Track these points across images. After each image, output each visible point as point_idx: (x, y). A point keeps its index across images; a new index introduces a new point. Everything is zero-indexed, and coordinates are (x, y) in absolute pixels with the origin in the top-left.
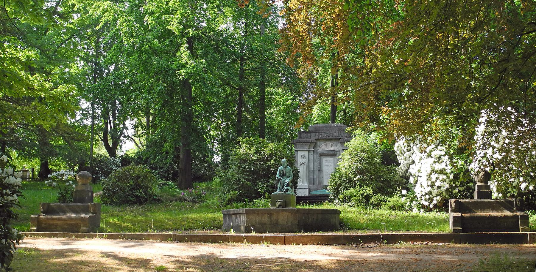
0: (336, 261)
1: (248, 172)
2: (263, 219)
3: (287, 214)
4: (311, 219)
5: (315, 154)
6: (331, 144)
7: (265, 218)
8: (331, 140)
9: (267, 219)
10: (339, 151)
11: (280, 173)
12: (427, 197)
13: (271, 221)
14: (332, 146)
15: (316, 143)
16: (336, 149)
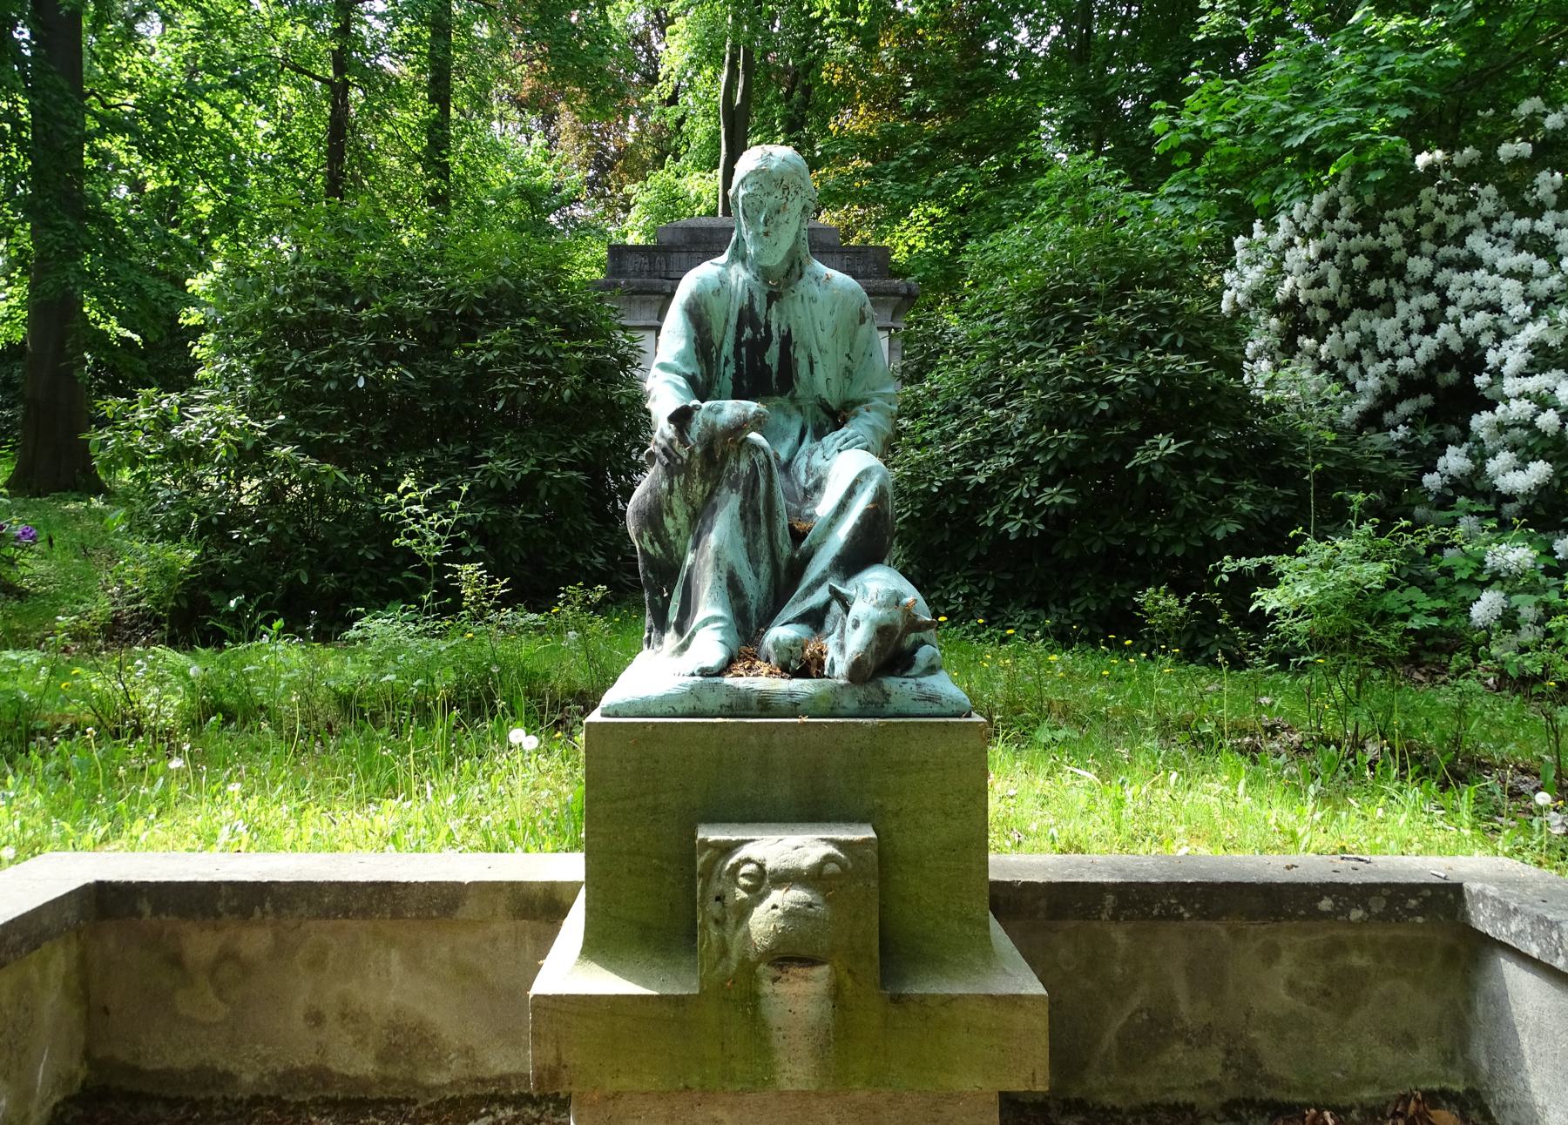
1: (331, 399)
11: (702, 343)
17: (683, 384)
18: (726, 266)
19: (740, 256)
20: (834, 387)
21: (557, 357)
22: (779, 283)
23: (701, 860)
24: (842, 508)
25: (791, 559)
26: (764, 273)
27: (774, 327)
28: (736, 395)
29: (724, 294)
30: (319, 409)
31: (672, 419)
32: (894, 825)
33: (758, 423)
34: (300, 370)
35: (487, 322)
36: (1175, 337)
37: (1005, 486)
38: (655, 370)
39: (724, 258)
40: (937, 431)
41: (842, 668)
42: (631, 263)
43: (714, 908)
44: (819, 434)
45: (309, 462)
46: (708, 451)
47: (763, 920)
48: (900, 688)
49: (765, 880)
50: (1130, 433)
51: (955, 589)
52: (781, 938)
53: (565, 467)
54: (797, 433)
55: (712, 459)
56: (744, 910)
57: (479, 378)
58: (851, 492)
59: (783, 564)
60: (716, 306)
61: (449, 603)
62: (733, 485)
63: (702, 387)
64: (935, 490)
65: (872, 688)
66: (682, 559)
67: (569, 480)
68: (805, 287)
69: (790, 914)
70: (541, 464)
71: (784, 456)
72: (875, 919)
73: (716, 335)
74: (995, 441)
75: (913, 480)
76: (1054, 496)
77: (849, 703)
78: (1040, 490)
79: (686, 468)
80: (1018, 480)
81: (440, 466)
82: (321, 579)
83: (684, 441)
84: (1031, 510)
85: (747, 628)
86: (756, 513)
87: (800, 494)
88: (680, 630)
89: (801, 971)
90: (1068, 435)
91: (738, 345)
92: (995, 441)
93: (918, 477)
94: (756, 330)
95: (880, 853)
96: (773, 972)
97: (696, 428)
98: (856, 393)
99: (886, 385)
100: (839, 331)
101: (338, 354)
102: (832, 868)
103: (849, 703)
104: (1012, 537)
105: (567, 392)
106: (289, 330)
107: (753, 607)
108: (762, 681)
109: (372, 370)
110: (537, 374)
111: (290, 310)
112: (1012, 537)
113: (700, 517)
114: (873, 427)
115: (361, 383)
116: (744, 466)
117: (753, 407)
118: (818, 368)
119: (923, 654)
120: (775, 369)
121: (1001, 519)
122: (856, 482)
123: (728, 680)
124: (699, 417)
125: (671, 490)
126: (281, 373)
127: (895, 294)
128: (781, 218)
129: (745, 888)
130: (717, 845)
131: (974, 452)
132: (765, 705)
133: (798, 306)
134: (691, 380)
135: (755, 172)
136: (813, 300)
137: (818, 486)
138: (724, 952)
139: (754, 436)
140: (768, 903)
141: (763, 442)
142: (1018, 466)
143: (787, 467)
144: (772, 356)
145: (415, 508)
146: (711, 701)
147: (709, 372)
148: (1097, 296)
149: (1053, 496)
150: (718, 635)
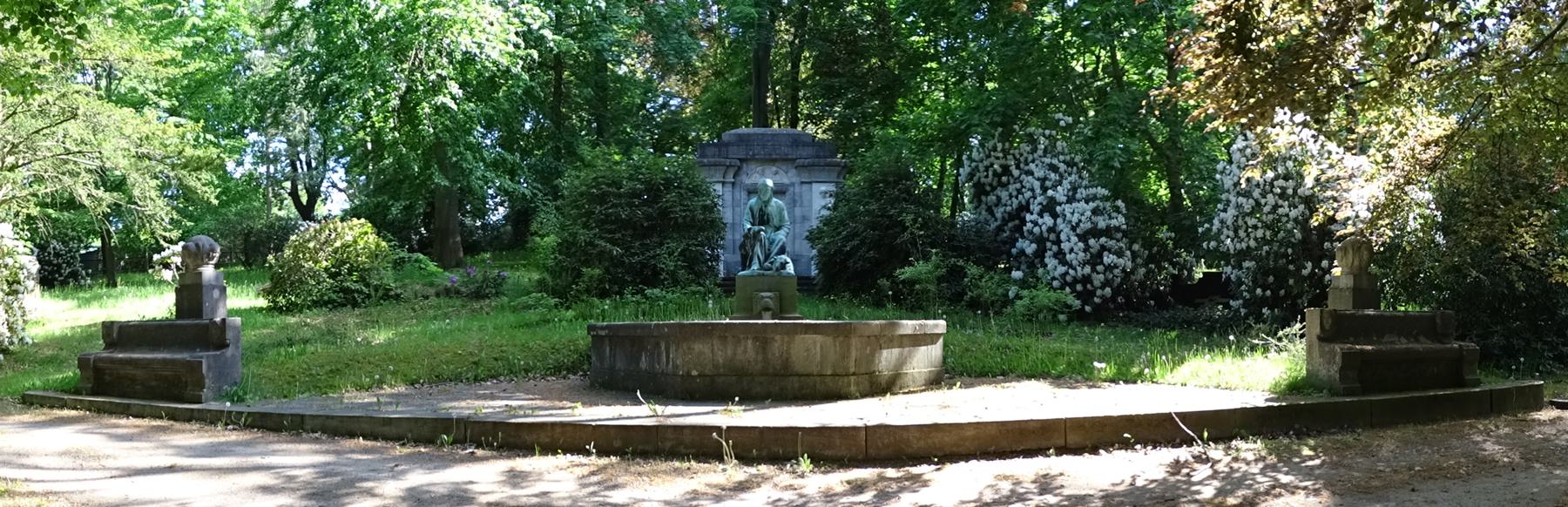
0: (847, 487)
1: (613, 223)
2: (740, 357)
3: (819, 338)
7: (748, 352)
8: (773, 161)
10: (793, 184)
12: (1079, 287)
15: (740, 168)
16: (786, 181)
61: (676, 282)
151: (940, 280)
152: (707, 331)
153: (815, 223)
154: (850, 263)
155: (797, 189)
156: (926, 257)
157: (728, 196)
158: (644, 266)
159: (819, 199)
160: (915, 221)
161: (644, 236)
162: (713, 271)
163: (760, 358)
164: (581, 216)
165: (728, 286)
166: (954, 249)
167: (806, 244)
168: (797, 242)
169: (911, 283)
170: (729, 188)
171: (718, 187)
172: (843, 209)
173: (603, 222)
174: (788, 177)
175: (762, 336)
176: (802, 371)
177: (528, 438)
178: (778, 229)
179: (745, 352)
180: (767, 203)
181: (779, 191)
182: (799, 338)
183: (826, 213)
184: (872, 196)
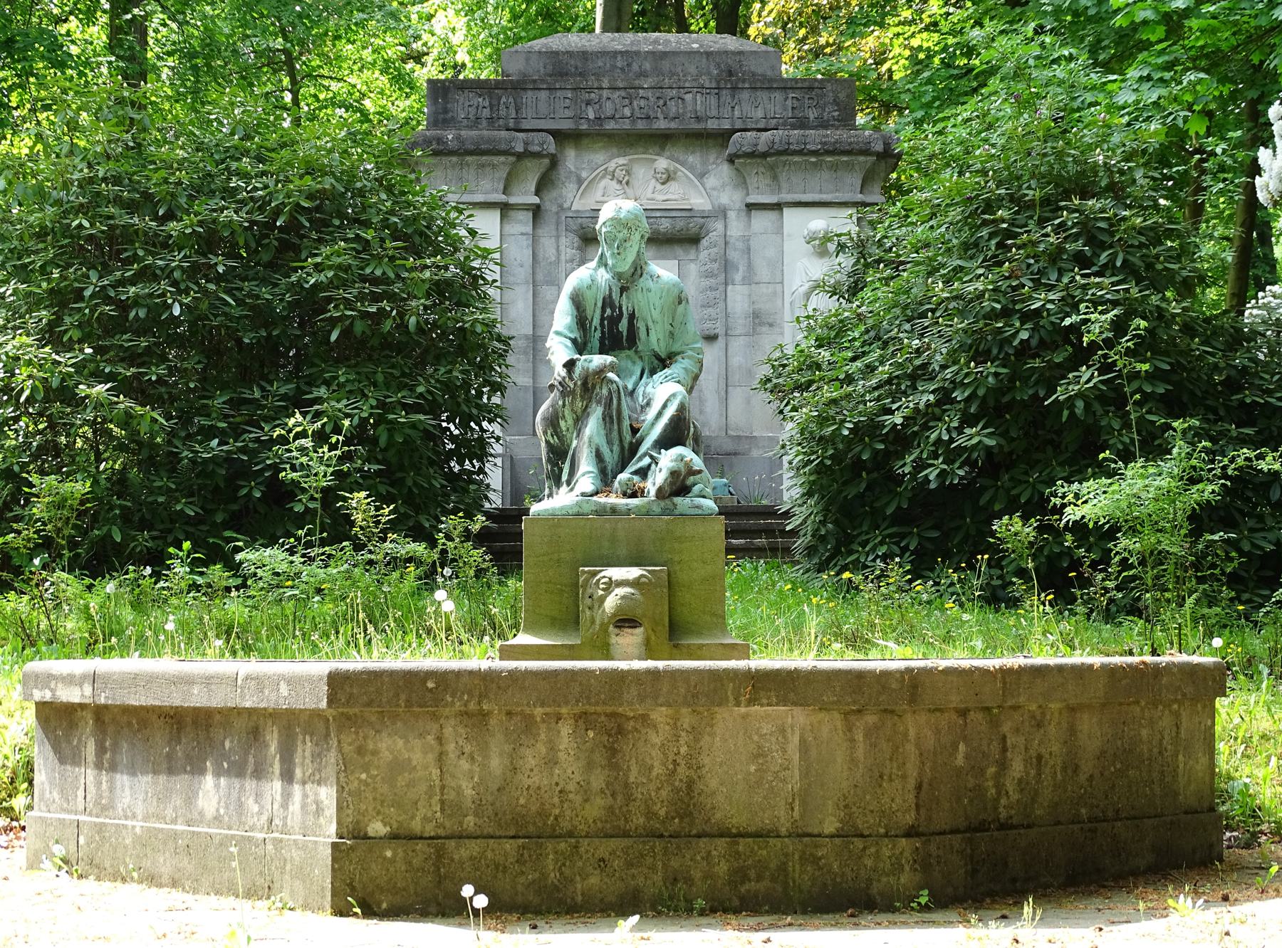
1: (141, 329)
2: (532, 772)
3: (797, 717)
4: (1017, 768)
5: (546, 231)
6: (662, 163)
7: (556, 767)
8: (661, 140)
9: (570, 768)
11: (582, 321)
13: (620, 789)
14: (668, 178)
15: (554, 162)
16: (699, 202)
17: (569, 343)
18: (595, 270)
19: (603, 263)
20: (662, 344)
21: (398, 276)
22: (629, 280)
23: (581, 579)
24: (660, 414)
25: (631, 443)
26: (619, 276)
27: (624, 308)
28: (603, 351)
29: (594, 288)
30: (125, 340)
31: (564, 366)
32: (677, 568)
33: (612, 367)
34: (102, 294)
35: (314, 235)
36: (1114, 255)
37: (926, 427)
38: (552, 335)
39: (593, 264)
40: (859, 364)
41: (653, 492)
42: (463, 106)
43: (588, 601)
44: (653, 372)
45: (124, 403)
46: (585, 384)
47: (611, 603)
48: (682, 502)
49: (611, 585)
50: (1052, 366)
51: (873, 549)
52: (619, 609)
53: (409, 409)
54: (639, 373)
55: (587, 388)
56: (602, 600)
57: (311, 303)
58: (665, 406)
59: (626, 446)
60: (589, 296)
61: (338, 528)
62: (599, 402)
63: (580, 347)
64: (846, 432)
65: (667, 501)
66: (569, 446)
67: (413, 426)
68: (644, 282)
69: (623, 598)
70: (382, 405)
71: (630, 387)
72: (666, 607)
73: (589, 313)
74: (920, 374)
75: (822, 420)
76: (973, 436)
77: (657, 509)
78: (960, 430)
79: (573, 392)
80: (940, 419)
81: (263, 407)
82: (134, 539)
83: (571, 378)
84: (952, 455)
85: (606, 477)
86: (611, 417)
87: (639, 409)
88: (568, 483)
89: (630, 630)
90: (990, 368)
91: (602, 319)
92: (920, 374)
93: (827, 419)
94: (613, 311)
95: (669, 575)
96: (616, 631)
97: (578, 370)
98: (676, 348)
99: (696, 342)
100: (666, 309)
101: (147, 275)
102: (643, 580)
103: (657, 509)
104: (933, 486)
105: (413, 320)
106: (75, 249)
107: (609, 468)
108: (613, 500)
109: (188, 294)
110: (376, 298)
111: (86, 224)
112: (933, 486)
113: (580, 420)
114: (685, 369)
115: (177, 311)
116: (605, 391)
117: (609, 359)
118: (652, 332)
119: (696, 489)
120: (625, 334)
121: (920, 465)
122: (667, 400)
123: (595, 498)
124: (579, 364)
125: (564, 405)
126: (81, 299)
127: (866, 152)
128: (628, 244)
129: (603, 589)
130: (589, 572)
131: (894, 387)
132: (614, 510)
133: (640, 295)
134: (574, 341)
135: (612, 219)
136: (649, 290)
137: (648, 404)
138: (593, 622)
139: (611, 375)
140: (613, 594)
141: (616, 379)
142: (938, 403)
143: (632, 393)
144: (623, 326)
145: (303, 441)
146: (587, 508)
147: (585, 336)
148: (1031, 205)
149: (971, 437)
150: (591, 480)
151: (1201, 520)
152: (1110, 81)
153: (791, 339)
154: (905, 467)
155: (736, 227)
156: (1154, 448)
157: (519, 252)
158: (237, 470)
159: (798, 259)
160: (1119, 327)
161: (246, 378)
162: (466, 492)
163: (598, 780)
164: (34, 303)
165: (504, 541)
166: (1246, 414)
167: (763, 404)
168: (737, 396)
169: (1099, 536)
170: (521, 224)
171: (487, 223)
172: (877, 296)
173: (116, 325)
174: (698, 187)
175: (606, 713)
176: (739, 820)
177: (566, 652)
178: (662, 362)
179: (551, 761)
180: (629, 280)
181: (675, 236)
182: (729, 717)
183: (824, 304)
184: (970, 248)
